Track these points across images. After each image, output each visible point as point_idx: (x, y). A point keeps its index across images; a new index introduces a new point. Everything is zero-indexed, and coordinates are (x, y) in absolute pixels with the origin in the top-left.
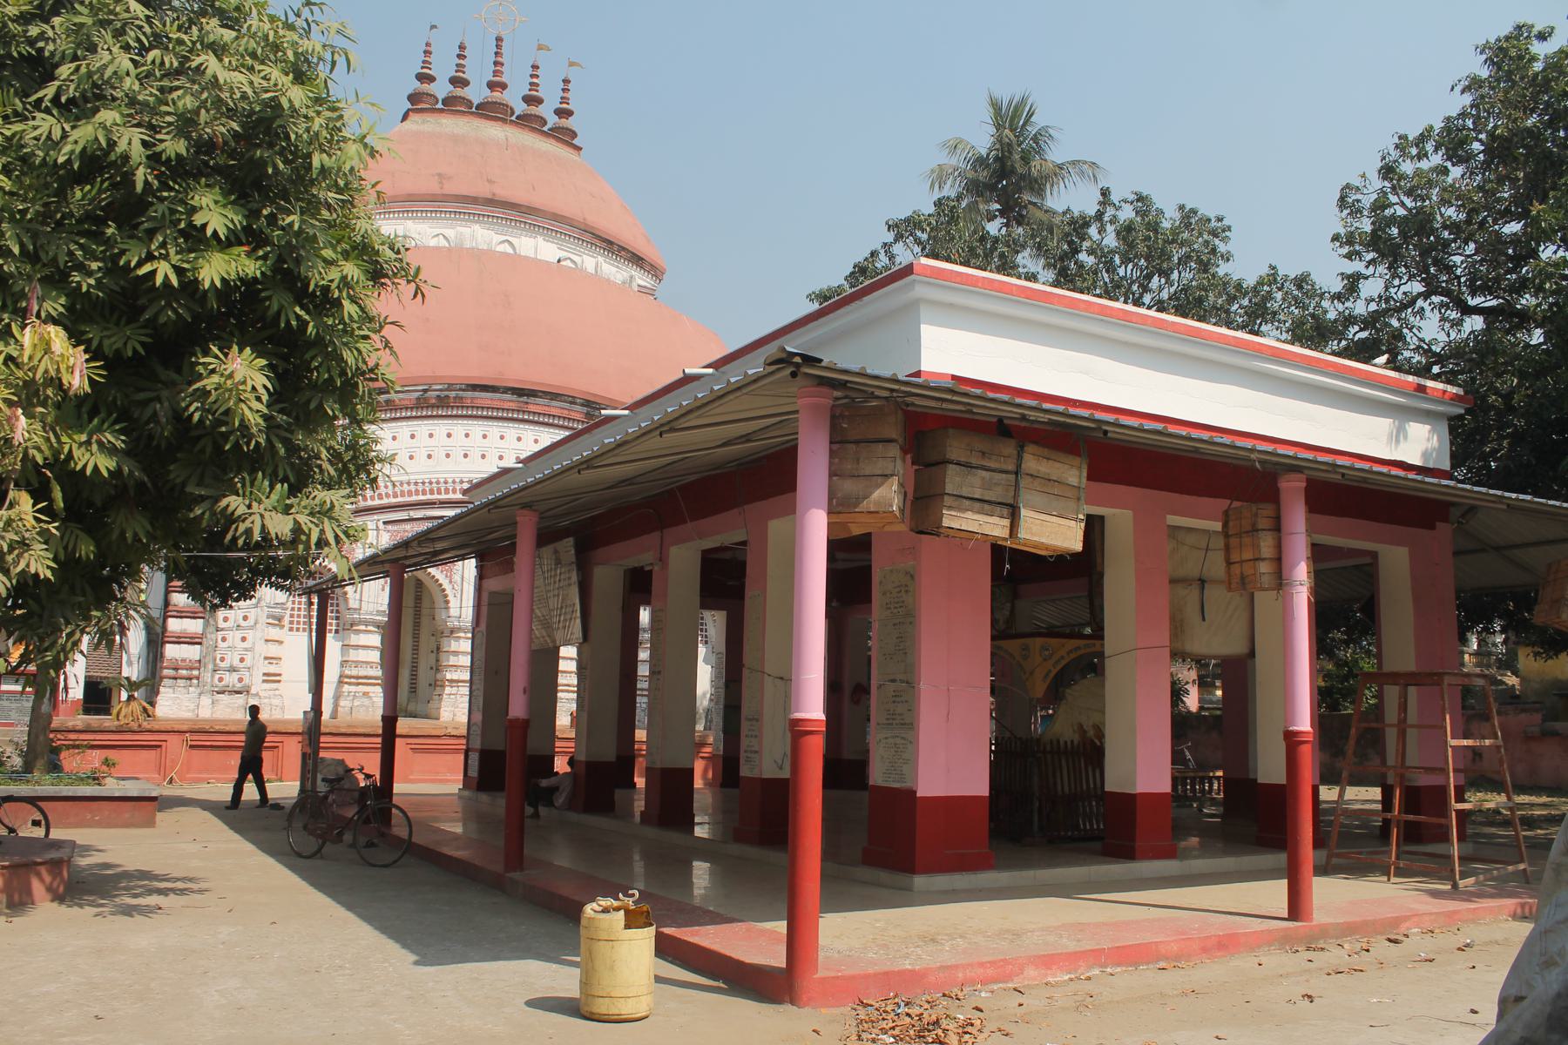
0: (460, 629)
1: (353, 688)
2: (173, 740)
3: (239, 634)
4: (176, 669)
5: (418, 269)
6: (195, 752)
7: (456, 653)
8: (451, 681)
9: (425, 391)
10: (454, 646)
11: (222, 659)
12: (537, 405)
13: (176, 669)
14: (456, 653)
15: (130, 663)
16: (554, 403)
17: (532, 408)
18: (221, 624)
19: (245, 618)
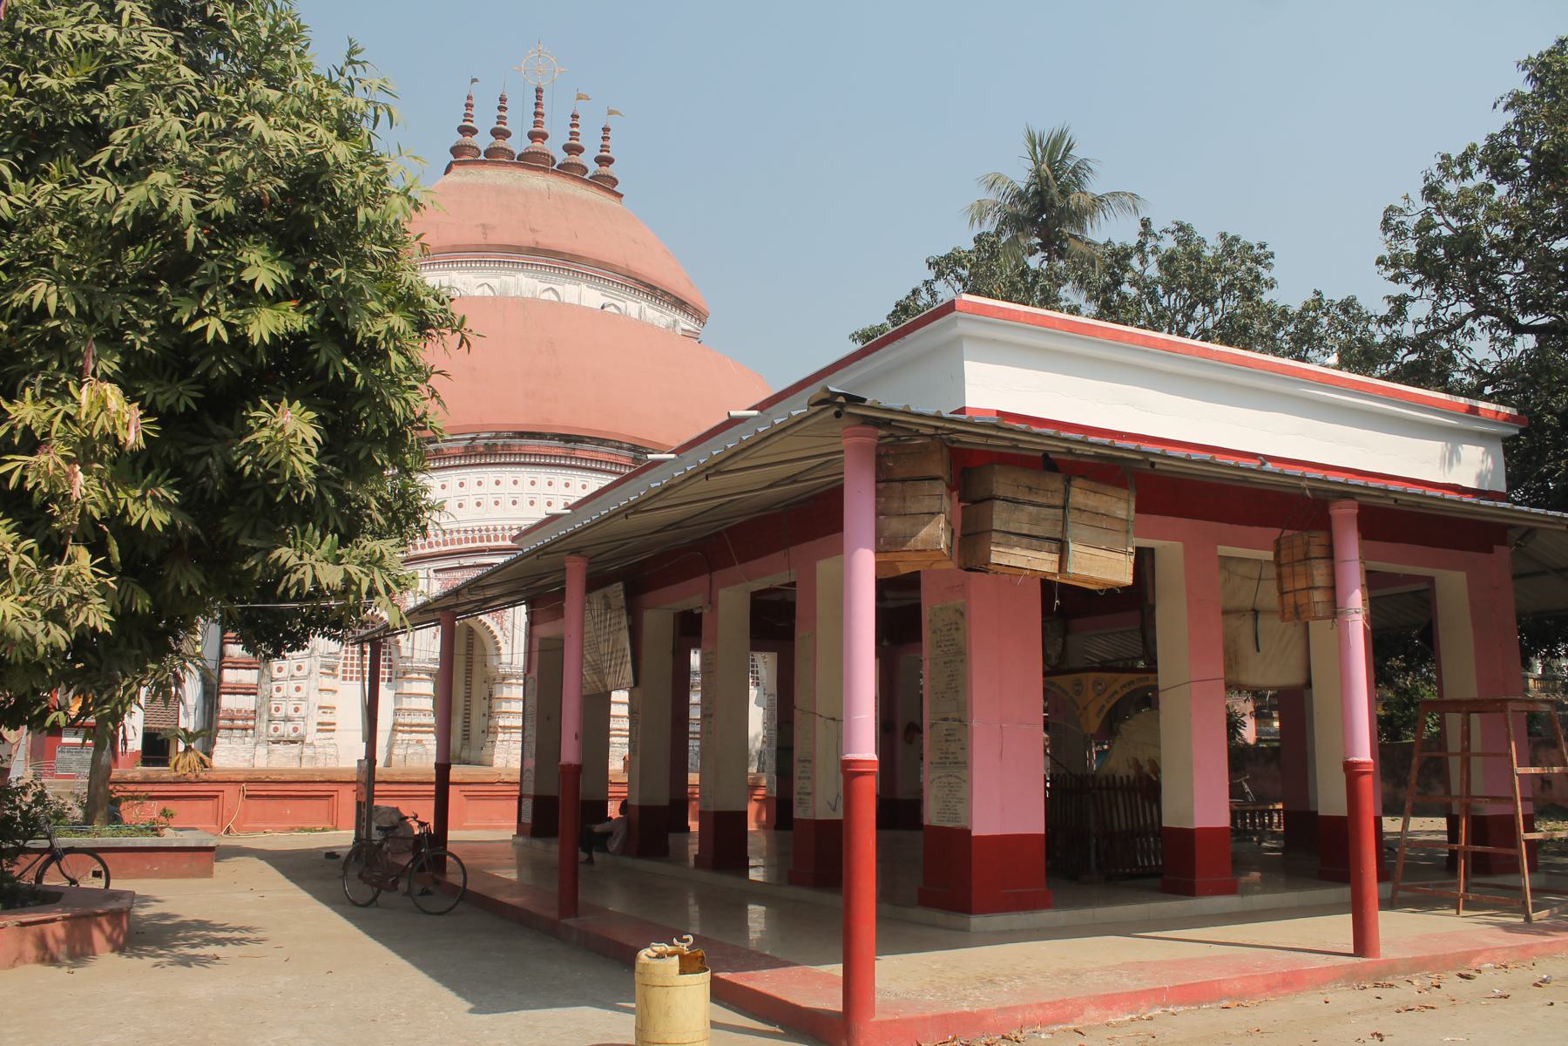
0: (512, 676)
1: (406, 736)
2: (230, 790)
3: (293, 684)
4: (232, 720)
5: (463, 319)
6: (251, 802)
7: (508, 700)
8: (504, 727)
9: (473, 439)
10: (506, 692)
11: (277, 709)
12: (584, 451)
13: (232, 720)
14: (508, 700)
15: (187, 715)
16: (601, 448)
17: (578, 454)
18: (276, 675)
19: (299, 668)
